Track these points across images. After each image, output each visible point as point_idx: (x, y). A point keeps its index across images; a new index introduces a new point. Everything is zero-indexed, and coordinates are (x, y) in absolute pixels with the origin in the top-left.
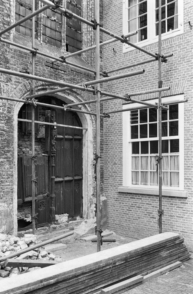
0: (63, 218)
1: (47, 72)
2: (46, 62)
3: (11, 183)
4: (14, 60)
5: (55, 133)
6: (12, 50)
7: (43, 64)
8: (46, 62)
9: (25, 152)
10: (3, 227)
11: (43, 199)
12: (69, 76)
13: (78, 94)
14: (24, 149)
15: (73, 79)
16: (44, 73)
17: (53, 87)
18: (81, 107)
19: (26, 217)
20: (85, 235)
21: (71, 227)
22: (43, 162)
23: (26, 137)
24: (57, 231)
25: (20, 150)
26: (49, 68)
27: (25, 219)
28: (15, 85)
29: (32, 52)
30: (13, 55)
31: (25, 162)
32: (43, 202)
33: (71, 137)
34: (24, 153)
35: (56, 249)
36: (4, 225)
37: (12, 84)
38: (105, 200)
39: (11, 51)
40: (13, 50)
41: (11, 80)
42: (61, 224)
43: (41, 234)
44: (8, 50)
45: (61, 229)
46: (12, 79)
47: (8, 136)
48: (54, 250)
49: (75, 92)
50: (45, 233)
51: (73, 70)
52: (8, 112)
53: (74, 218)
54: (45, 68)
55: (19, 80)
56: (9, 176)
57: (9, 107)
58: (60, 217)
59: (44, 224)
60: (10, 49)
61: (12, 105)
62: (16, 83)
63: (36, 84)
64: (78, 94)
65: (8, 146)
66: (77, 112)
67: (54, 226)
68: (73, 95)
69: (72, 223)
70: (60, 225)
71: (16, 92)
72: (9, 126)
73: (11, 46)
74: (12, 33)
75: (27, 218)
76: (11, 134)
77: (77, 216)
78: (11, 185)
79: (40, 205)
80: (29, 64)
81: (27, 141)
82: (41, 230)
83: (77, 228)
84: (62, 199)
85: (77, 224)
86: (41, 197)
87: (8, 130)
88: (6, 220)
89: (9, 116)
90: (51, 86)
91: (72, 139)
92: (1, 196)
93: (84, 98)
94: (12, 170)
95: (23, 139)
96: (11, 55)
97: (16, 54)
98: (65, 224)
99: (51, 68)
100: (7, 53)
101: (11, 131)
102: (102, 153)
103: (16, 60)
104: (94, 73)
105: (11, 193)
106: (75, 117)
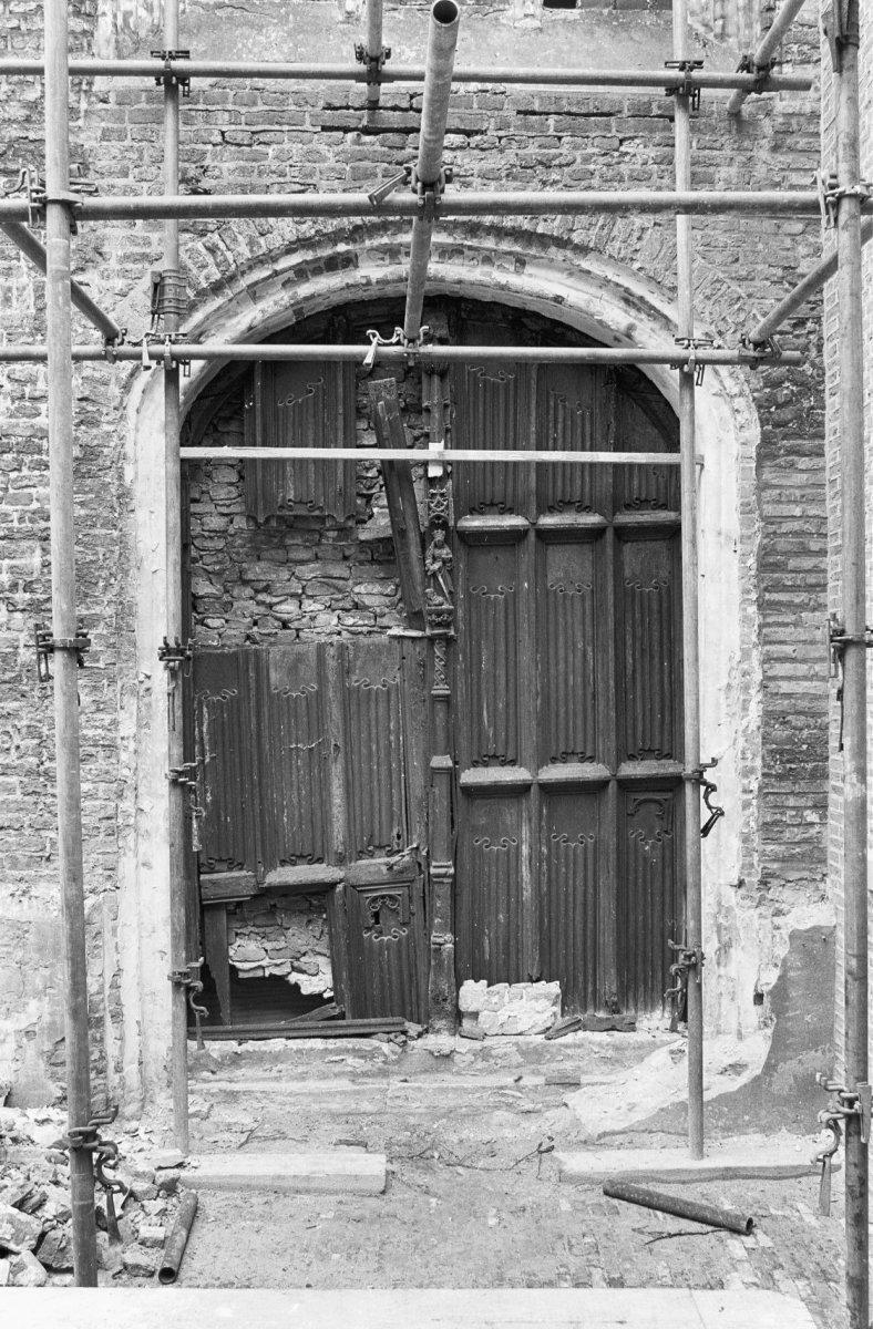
0: (520, 1008)
1: (331, 163)
2: (329, 107)
3: (102, 786)
4: (115, 147)
5: (439, 504)
6: (105, 101)
7: (307, 126)
8: (329, 107)
9: (290, 621)
10: (33, 1005)
11: (391, 883)
12: (502, 151)
13: (583, 250)
14: (288, 608)
15: (541, 163)
16: (311, 175)
17: (385, 240)
18: (631, 327)
19: (294, 969)
20: (620, 1138)
21: (568, 1065)
22: (394, 677)
23: (299, 541)
24: (458, 1073)
25: (262, 609)
26: (350, 136)
27: (294, 978)
28: (124, 273)
29: (672, 87)
30: (110, 125)
31: (274, 676)
32: (391, 897)
33: (592, 519)
34: (285, 625)
35: (301, 1185)
36: (38, 994)
37: (105, 276)
38: (817, 929)
39: (101, 106)
40: (112, 98)
41: (100, 254)
42: (488, 1042)
43: (336, 1075)
44: (83, 106)
45: (492, 1072)
46: (104, 250)
47: (86, 545)
48: (285, 1184)
49: (562, 243)
50: (365, 1074)
51: (536, 107)
52: (82, 422)
53: (628, 1014)
54: (321, 143)
55: (148, 243)
56: (92, 750)
57: (86, 393)
58: (495, 999)
59: (373, 1021)
60: (93, 99)
61: (106, 384)
62: (129, 266)
63: (251, 243)
64: (583, 250)
65: (86, 595)
66: (643, 367)
67: (442, 1041)
68: (551, 264)
69: (579, 1046)
70: (477, 1045)
71: (129, 311)
72: (91, 491)
73: (100, 83)
74: (104, 14)
75: (304, 977)
76: (104, 531)
77: (649, 1005)
78: (100, 794)
79: (376, 916)
80: (210, 147)
81: (302, 562)
82: (338, 1051)
83: (613, 1078)
84: (527, 894)
85: (610, 1053)
86: (379, 871)
87: (83, 512)
88: (47, 972)
89: (85, 439)
90: (371, 237)
91: (595, 534)
92: (48, 849)
93: (636, 265)
94: (107, 719)
95: (280, 555)
96: (103, 124)
97: (131, 112)
98: (517, 1044)
99: (367, 131)
100: (80, 123)
101: (98, 516)
102: (814, 610)
103: (128, 143)
104: (662, 91)
105: (102, 835)
106: (635, 400)
